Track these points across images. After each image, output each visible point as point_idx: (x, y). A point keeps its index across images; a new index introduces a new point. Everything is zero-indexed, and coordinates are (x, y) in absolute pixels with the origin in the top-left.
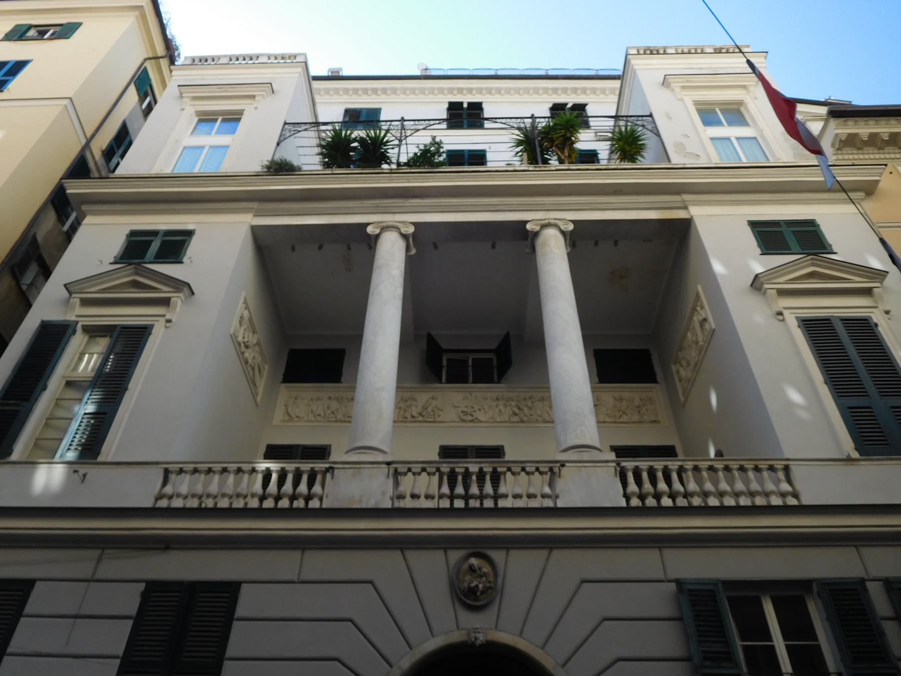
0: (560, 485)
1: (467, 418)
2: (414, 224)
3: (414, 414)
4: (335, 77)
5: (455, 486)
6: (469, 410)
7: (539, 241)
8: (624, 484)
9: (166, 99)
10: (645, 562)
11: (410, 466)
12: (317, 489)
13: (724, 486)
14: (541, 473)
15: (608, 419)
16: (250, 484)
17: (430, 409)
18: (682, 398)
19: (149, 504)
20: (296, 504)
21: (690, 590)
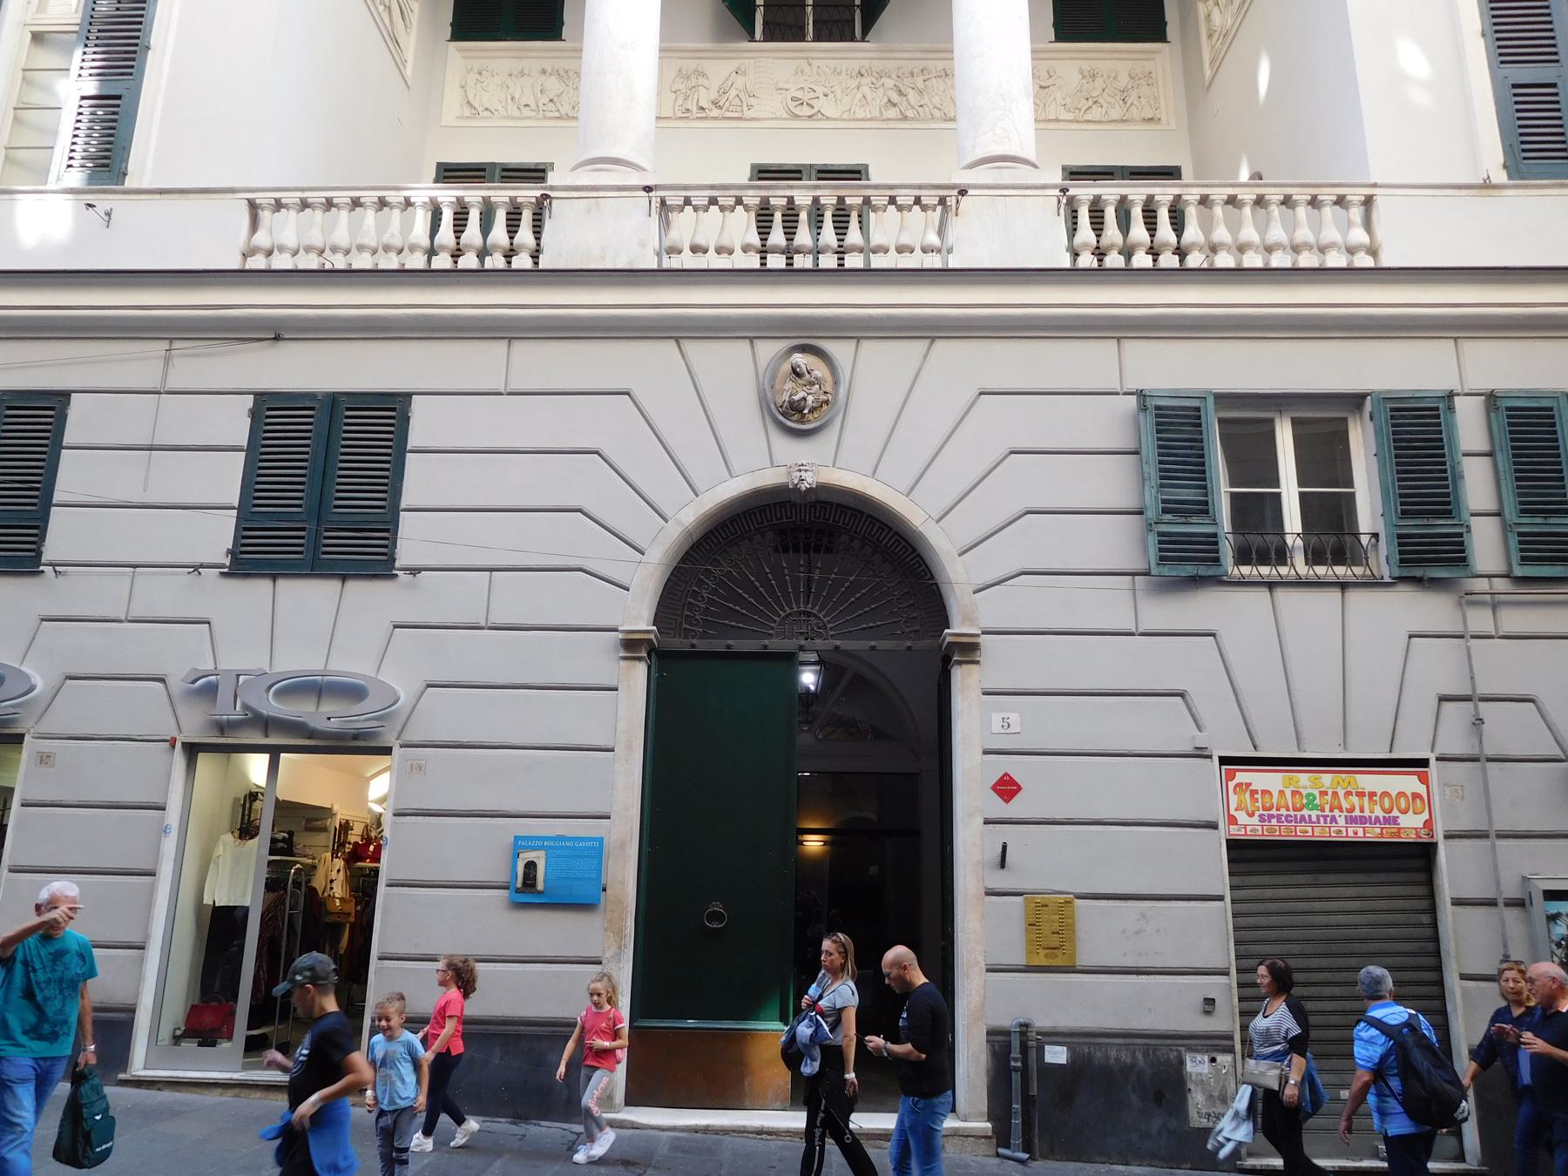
0: (956, 228)
1: (803, 110)
6: (806, 97)
8: (1073, 228)
10: (1091, 362)
11: (688, 193)
13: (1249, 233)
14: (924, 208)
15: (1064, 115)
16: (407, 227)
17: (733, 93)
18: (1208, 73)
19: (234, 263)
20: (463, 263)
21: (1158, 408)
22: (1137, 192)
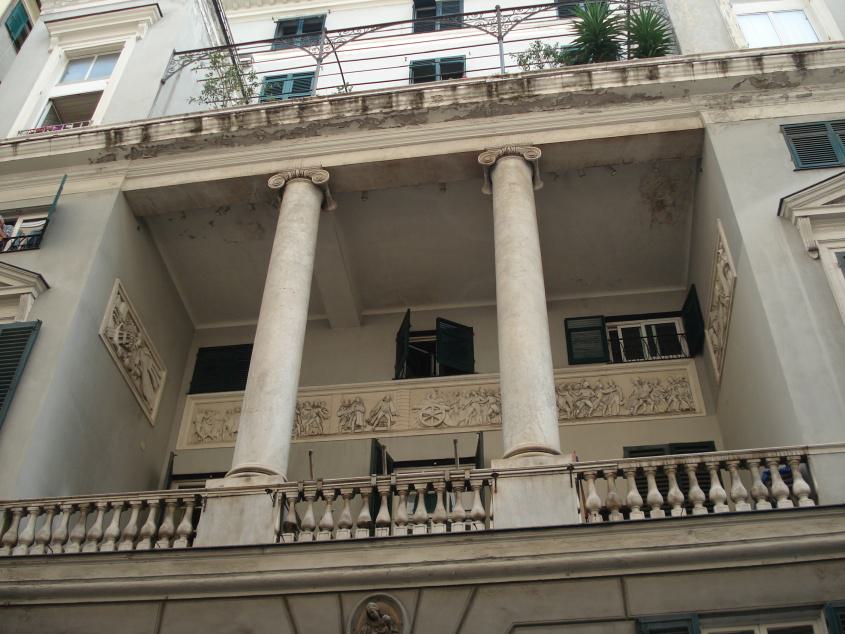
2: (541, 146)
5: (688, 489)
7: (497, 175)
18: (718, 375)
22: (670, 461)
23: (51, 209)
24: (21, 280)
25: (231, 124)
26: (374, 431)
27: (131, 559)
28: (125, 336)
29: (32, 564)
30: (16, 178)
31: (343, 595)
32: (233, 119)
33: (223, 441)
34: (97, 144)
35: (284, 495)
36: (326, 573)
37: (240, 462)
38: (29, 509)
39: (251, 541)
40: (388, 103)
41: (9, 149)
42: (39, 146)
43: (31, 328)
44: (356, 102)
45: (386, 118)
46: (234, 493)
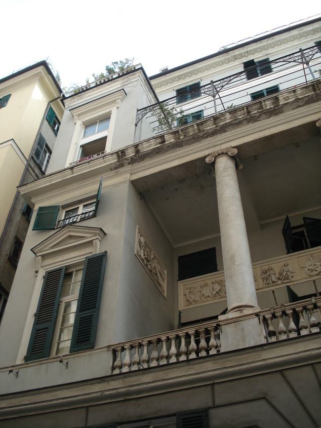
3: (274, 279)
4: (166, 72)
9: (65, 119)
12: (213, 342)
20: (211, 353)
23: (96, 196)
24: (92, 233)
25: (180, 135)
26: (283, 283)
27: (189, 364)
28: (146, 254)
29: (135, 375)
30: (75, 185)
31: (314, 365)
32: (180, 133)
33: (202, 302)
34: (113, 160)
35: (264, 317)
36: (302, 354)
37: (232, 304)
38: (125, 347)
39: (252, 344)
40: (261, 106)
41: (69, 171)
42: (84, 167)
43: (103, 255)
44: (243, 110)
45: (261, 114)
46: (236, 320)
